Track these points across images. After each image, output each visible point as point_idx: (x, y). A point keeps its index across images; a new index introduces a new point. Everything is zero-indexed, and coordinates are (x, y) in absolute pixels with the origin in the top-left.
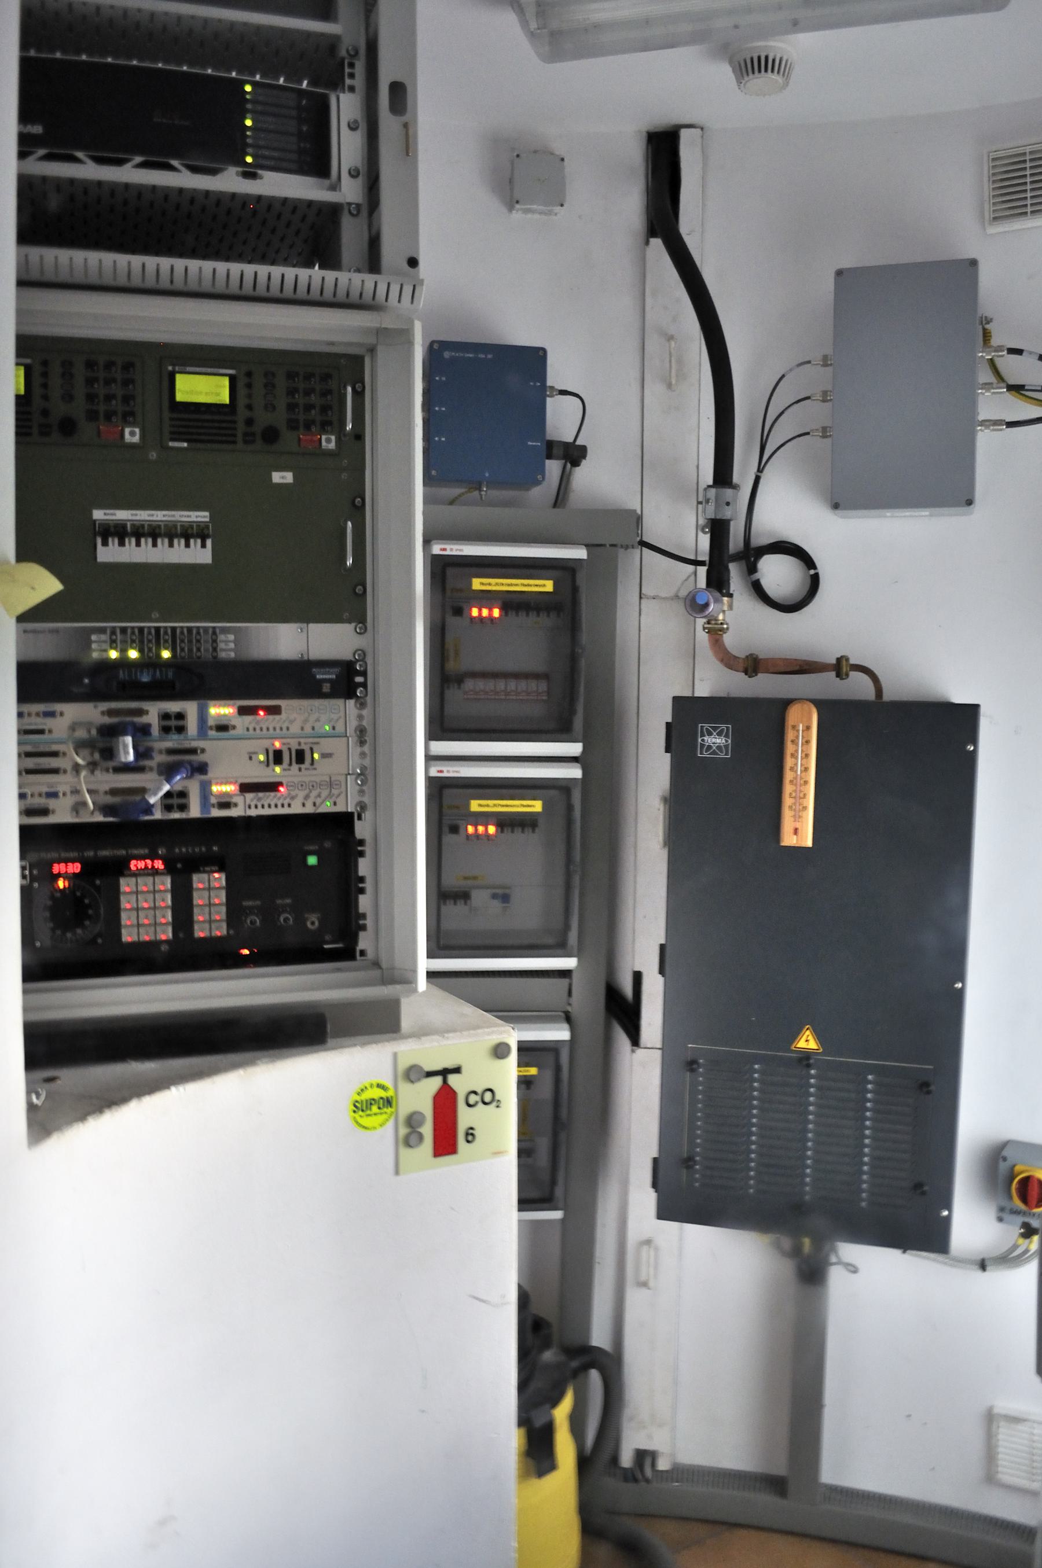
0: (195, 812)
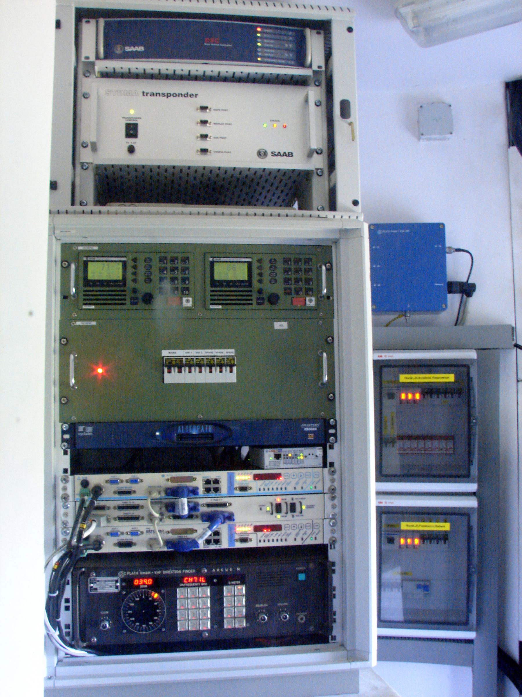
0: (225, 545)
